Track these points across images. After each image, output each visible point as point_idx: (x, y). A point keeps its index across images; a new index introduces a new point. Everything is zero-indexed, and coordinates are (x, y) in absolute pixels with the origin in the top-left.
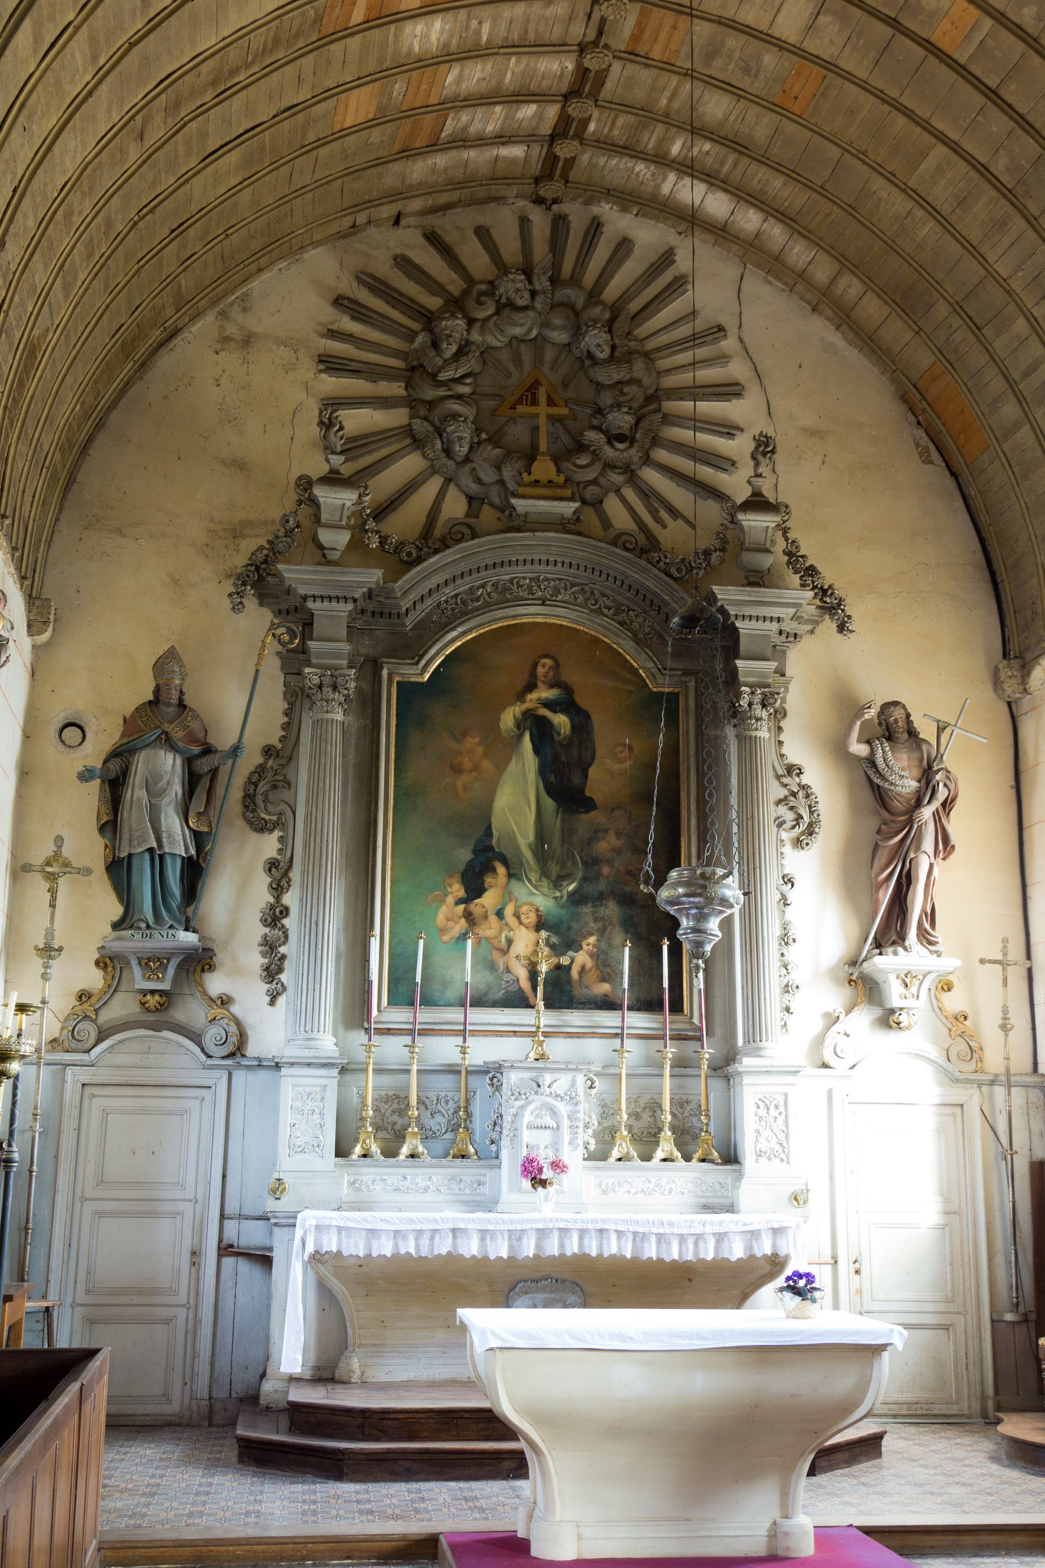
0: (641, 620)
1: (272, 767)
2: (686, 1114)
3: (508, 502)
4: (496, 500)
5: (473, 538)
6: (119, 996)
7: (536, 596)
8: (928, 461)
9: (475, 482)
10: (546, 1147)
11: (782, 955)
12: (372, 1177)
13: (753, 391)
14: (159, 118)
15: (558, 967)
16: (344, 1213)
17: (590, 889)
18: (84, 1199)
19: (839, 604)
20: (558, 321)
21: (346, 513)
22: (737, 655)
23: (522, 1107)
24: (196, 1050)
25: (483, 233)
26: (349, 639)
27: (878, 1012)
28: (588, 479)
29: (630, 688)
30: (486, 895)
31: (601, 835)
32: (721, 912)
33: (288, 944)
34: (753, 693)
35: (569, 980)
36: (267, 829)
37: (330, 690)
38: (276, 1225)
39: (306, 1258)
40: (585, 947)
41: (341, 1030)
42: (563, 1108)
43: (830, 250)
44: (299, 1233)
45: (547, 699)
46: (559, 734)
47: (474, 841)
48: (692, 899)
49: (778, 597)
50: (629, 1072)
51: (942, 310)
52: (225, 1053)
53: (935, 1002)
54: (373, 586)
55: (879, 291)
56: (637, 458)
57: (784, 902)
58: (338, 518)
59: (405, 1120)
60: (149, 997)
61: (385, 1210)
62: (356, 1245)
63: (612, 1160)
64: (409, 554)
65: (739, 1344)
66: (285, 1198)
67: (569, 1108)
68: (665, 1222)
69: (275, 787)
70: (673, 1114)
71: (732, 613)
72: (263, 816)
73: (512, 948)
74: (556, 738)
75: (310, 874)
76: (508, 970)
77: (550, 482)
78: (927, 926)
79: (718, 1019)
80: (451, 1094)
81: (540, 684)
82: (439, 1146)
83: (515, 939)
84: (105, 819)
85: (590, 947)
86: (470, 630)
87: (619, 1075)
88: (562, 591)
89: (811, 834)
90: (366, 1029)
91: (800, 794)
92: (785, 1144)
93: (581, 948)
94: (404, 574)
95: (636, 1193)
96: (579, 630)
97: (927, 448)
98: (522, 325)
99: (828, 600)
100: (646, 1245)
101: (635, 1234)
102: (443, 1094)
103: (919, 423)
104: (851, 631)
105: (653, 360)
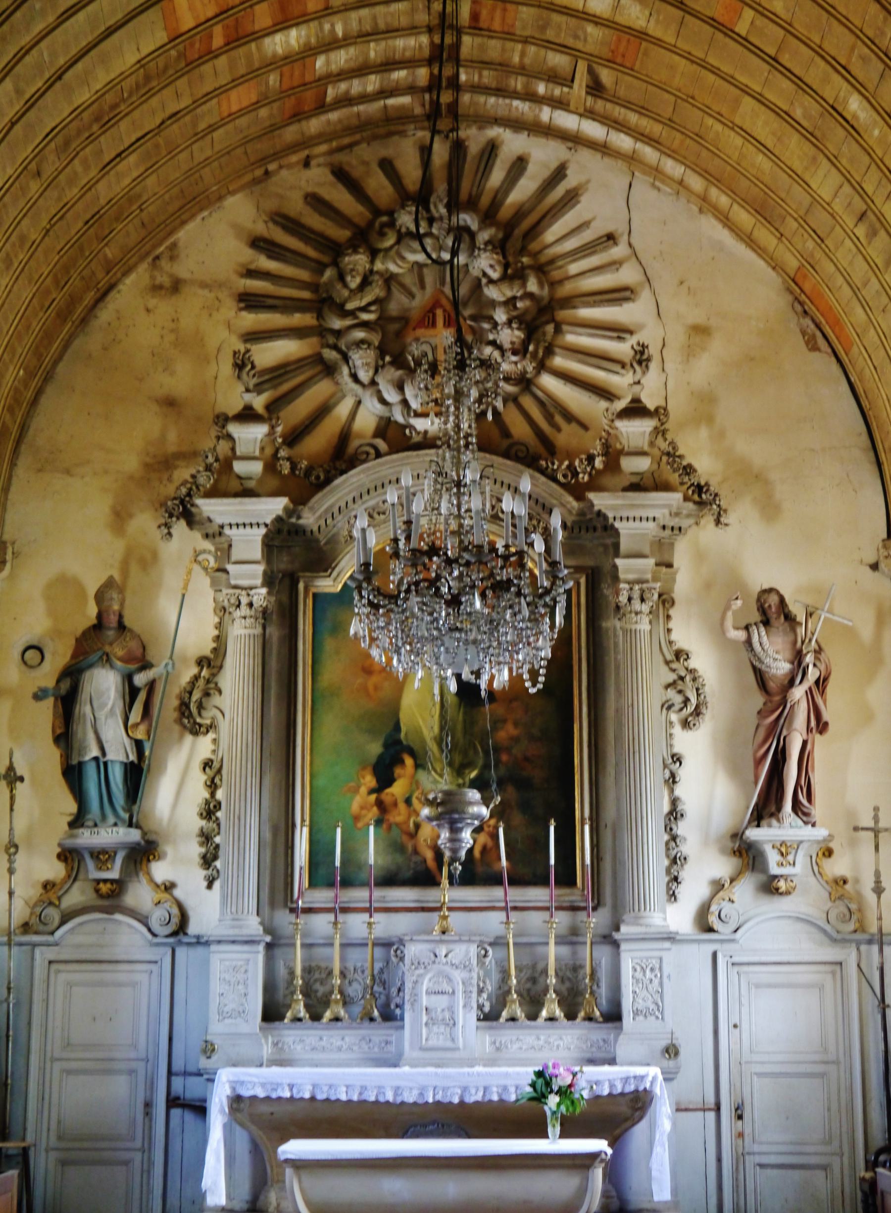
6: (77, 884)
8: (814, 348)
10: (443, 1010)
11: (671, 829)
13: (645, 296)
14: (52, 157)
18: (54, 1060)
19: (714, 500)
22: (617, 554)
23: (420, 976)
24: (144, 930)
25: (387, 166)
27: (762, 878)
34: (631, 589)
42: (458, 976)
43: (695, 167)
47: (384, 736)
53: (816, 868)
55: (742, 202)
56: (531, 368)
57: (673, 779)
60: (101, 885)
61: (303, 1066)
63: (540, 1021)
67: (465, 974)
70: (302, 978)
76: (416, 852)
78: (803, 799)
82: (357, 1009)
84: (59, 731)
91: (688, 678)
95: (526, 1050)
102: (359, 965)
104: (726, 525)
105: (545, 273)
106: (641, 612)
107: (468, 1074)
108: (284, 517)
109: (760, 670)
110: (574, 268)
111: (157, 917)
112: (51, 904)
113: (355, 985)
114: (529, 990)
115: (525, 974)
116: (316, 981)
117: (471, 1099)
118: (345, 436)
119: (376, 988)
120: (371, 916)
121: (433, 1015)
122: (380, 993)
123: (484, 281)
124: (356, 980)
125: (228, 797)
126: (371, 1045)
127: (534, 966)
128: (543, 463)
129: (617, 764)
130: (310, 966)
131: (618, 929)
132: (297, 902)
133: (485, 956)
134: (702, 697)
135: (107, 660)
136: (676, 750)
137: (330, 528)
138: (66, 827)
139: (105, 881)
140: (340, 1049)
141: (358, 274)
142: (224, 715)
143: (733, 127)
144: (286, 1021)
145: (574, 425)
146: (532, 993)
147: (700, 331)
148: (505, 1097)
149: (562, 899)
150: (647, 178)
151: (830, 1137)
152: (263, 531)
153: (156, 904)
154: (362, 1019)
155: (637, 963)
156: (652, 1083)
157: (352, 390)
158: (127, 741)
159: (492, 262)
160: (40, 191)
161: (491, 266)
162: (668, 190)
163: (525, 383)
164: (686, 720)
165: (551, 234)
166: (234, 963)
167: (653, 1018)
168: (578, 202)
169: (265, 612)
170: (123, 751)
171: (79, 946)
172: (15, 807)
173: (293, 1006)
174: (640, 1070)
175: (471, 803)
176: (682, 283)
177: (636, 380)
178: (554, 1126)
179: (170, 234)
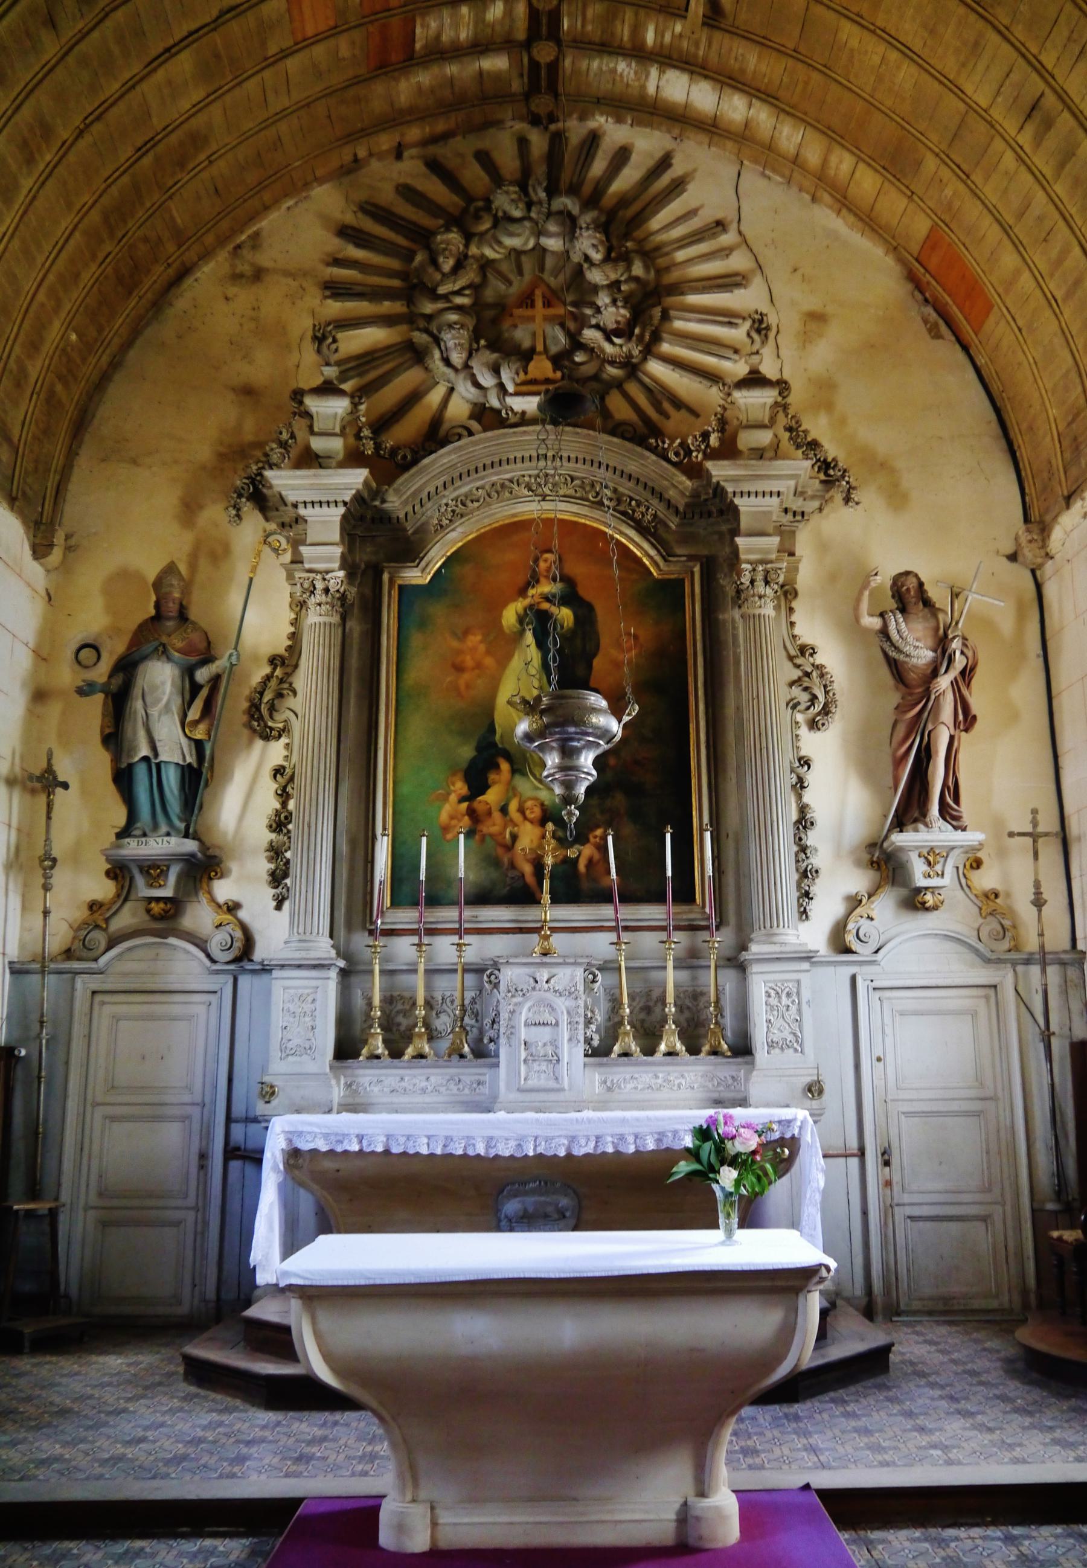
8: (938, 336)
10: (545, 1045)
11: (800, 839)
13: (757, 281)
18: (96, 1104)
19: (843, 476)
20: (552, 227)
25: (484, 158)
27: (903, 892)
34: (754, 570)
40: (592, 839)
42: (562, 1004)
51: (931, 164)
52: (228, 959)
53: (963, 881)
57: (800, 785)
60: (153, 905)
63: (658, 1056)
67: (570, 1003)
70: (382, 1009)
76: (512, 866)
82: (444, 1045)
83: (520, 834)
84: (107, 731)
85: (598, 840)
87: (619, 969)
91: (814, 674)
97: (936, 325)
98: (519, 235)
99: (831, 472)
102: (448, 994)
103: (926, 300)
105: (653, 260)
106: (765, 596)
107: (577, 1120)
108: (366, 495)
109: (895, 660)
110: (681, 255)
111: (217, 941)
112: (97, 927)
113: (444, 1018)
114: (643, 1021)
115: (640, 1003)
116: (398, 1012)
117: (579, 1151)
118: (437, 421)
119: (467, 1020)
120: (461, 938)
121: (534, 1050)
122: (472, 1027)
123: (586, 266)
125: (298, 806)
126: (461, 1086)
127: (648, 994)
128: (652, 441)
129: (738, 767)
130: (392, 996)
131: (744, 948)
132: (376, 922)
133: (594, 981)
134: (831, 694)
135: (163, 652)
136: (803, 753)
137: (418, 516)
138: (114, 838)
139: (158, 900)
140: (424, 1091)
141: (451, 254)
142: (297, 716)
143: (873, 30)
144: (361, 1058)
145: (683, 413)
146: (646, 1025)
147: (816, 318)
148: (621, 1149)
149: (679, 917)
150: (757, 167)
151: (990, 1184)
152: (342, 510)
153: (217, 927)
154: (450, 1056)
156: (801, 1128)
157: (444, 374)
158: (184, 741)
159: (595, 242)
160: (59, 55)
161: (594, 246)
162: (779, 179)
163: (632, 369)
164: (814, 720)
165: (656, 223)
166: (300, 991)
167: (791, 1050)
168: (684, 191)
169: (343, 598)
170: (180, 752)
171: (125, 974)
172: (54, 815)
173: (370, 1041)
174: (786, 1113)
175: (595, 710)
176: (795, 270)
177: (754, 349)
178: (728, 1216)
179: (253, 217)
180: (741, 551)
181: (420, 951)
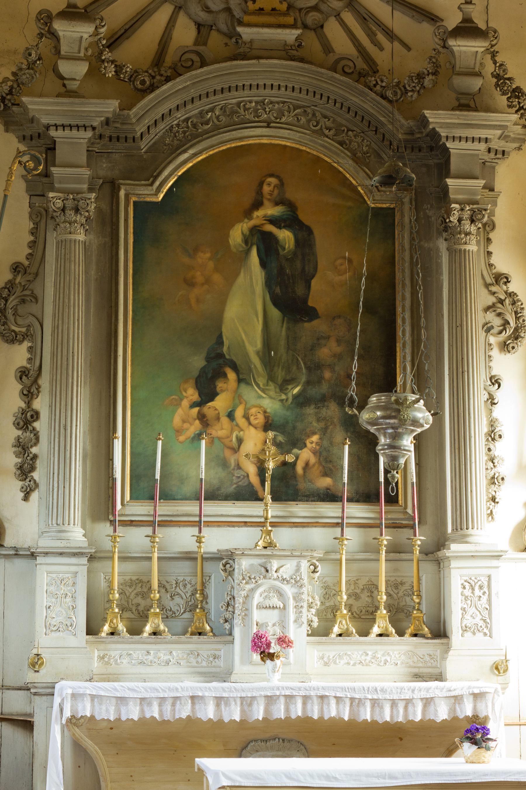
0: (359, 139)
1: (20, 283)
2: (401, 594)
3: (234, 29)
4: (223, 27)
5: (201, 67)
7: (261, 119)
9: (203, 10)
10: (274, 625)
11: (489, 450)
12: (118, 652)
15: (284, 464)
16: (95, 683)
17: (313, 392)
21: (84, 44)
22: (448, 175)
23: (253, 590)
26: (88, 165)
28: (309, 5)
29: (350, 204)
30: (218, 398)
31: (323, 342)
32: (413, 431)
33: (39, 445)
34: (462, 210)
35: (294, 476)
36: (18, 341)
37: (72, 213)
38: (35, 694)
39: (64, 722)
40: (309, 445)
41: (88, 522)
42: (289, 590)
44: (57, 700)
45: (272, 216)
46: (284, 249)
48: (388, 421)
49: (486, 120)
50: (348, 557)
54: (110, 115)
57: (492, 401)
58: (76, 49)
59: (148, 602)
61: (131, 681)
62: (107, 711)
63: (333, 636)
64: (143, 82)
65: (423, 782)
66: (43, 671)
67: (295, 590)
68: (378, 689)
69: (23, 301)
70: (388, 594)
71: (443, 134)
72: (13, 328)
73: (242, 447)
74: (281, 252)
75: (58, 383)
76: (239, 467)
77: (273, 9)
79: (429, 509)
80: (188, 579)
81: (266, 202)
82: (178, 625)
83: (245, 438)
85: (314, 445)
86: (200, 152)
87: (340, 560)
88: (286, 113)
89: (516, 338)
90: (111, 521)
91: (507, 301)
92: (488, 621)
93: (305, 446)
94: (139, 101)
95: (354, 665)
96: (301, 151)
100: (362, 709)
101: (352, 699)
102: (181, 579)
124: (178, 594)
126: (199, 660)
155: (465, 581)
164: (505, 343)
180: (450, 191)
181: (153, 542)
